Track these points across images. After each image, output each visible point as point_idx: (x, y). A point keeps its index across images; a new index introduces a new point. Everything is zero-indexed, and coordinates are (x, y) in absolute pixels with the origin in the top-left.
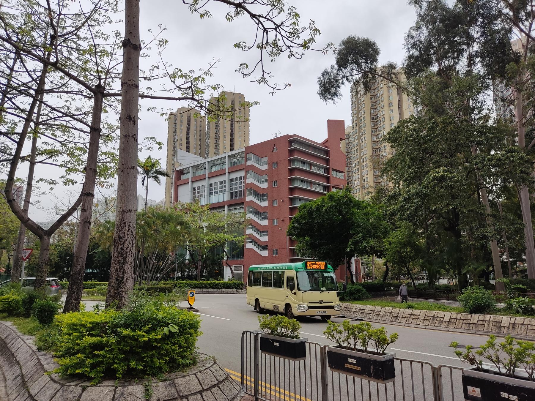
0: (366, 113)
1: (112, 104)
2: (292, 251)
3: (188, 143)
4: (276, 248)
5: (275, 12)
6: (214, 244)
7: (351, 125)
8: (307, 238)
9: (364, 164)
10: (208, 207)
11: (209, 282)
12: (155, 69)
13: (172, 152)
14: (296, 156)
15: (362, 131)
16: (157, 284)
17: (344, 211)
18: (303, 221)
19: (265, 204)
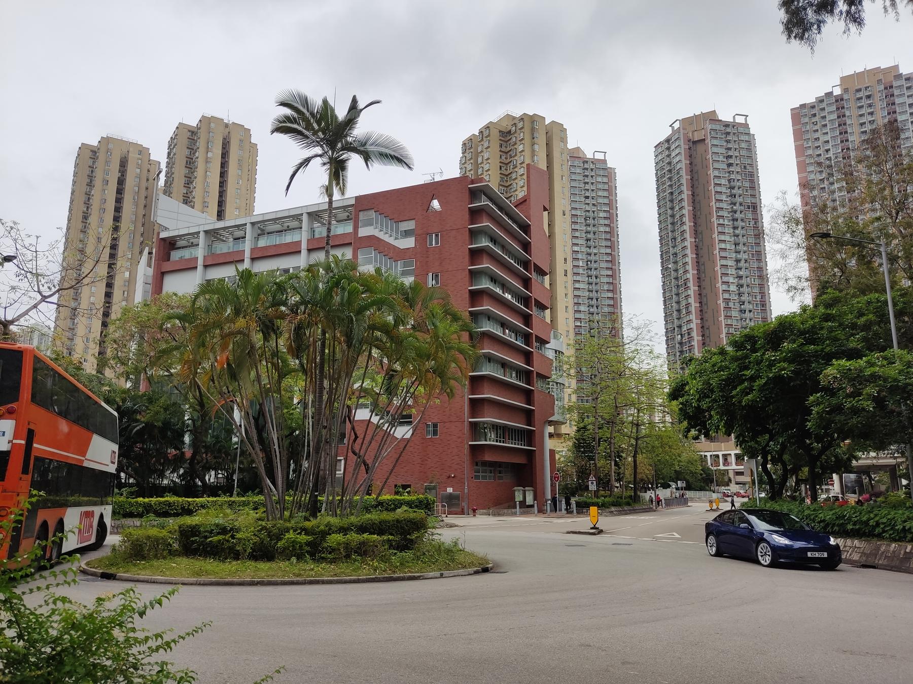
2: (474, 426)
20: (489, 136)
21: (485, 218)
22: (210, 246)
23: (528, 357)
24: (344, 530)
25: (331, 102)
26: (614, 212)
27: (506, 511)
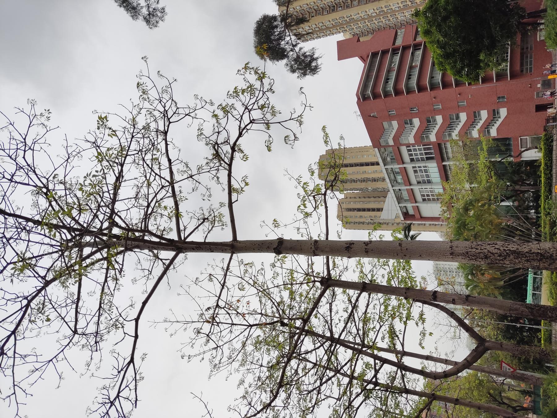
0: (328, 19)
1: (338, 274)
3: (373, 210)
4: (496, 99)
5: (235, 113)
6: (492, 173)
7: (342, 34)
8: (482, 57)
9: (385, 9)
10: (445, 183)
11: (543, 175)
12: (301, 230)
13: (385, 226)
14: (380, 90)
15: (348, 19)
16: (546, 234)
17: (444, 14)
18: (459, 65)
19: (439, 119)
22: (406, 201)
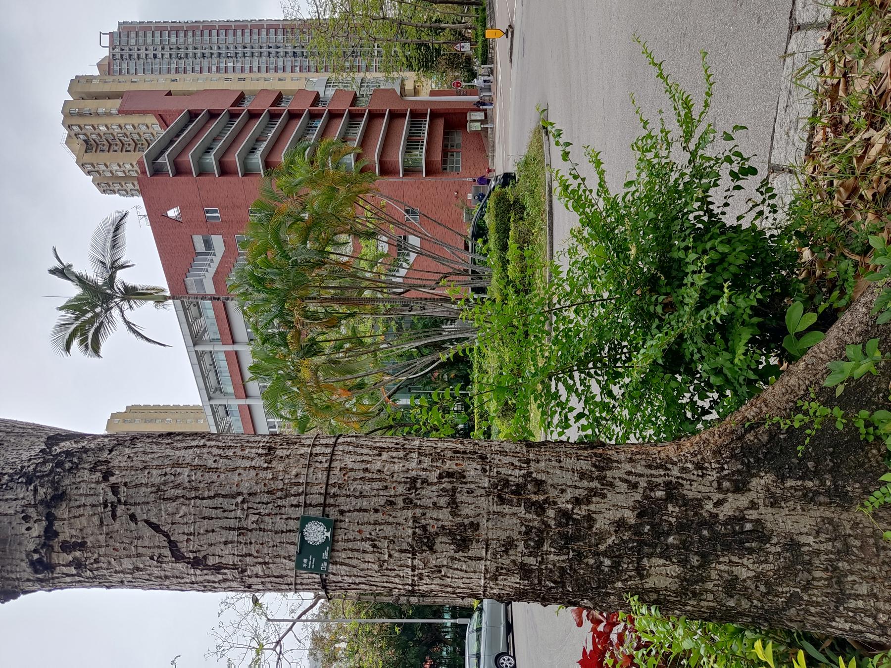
20: (92, 164)
21: (183, 159)
23: (334, 115)
24: (505, 263)
25: (63, 302)
26: (169, 26)
27: (490, 139)
